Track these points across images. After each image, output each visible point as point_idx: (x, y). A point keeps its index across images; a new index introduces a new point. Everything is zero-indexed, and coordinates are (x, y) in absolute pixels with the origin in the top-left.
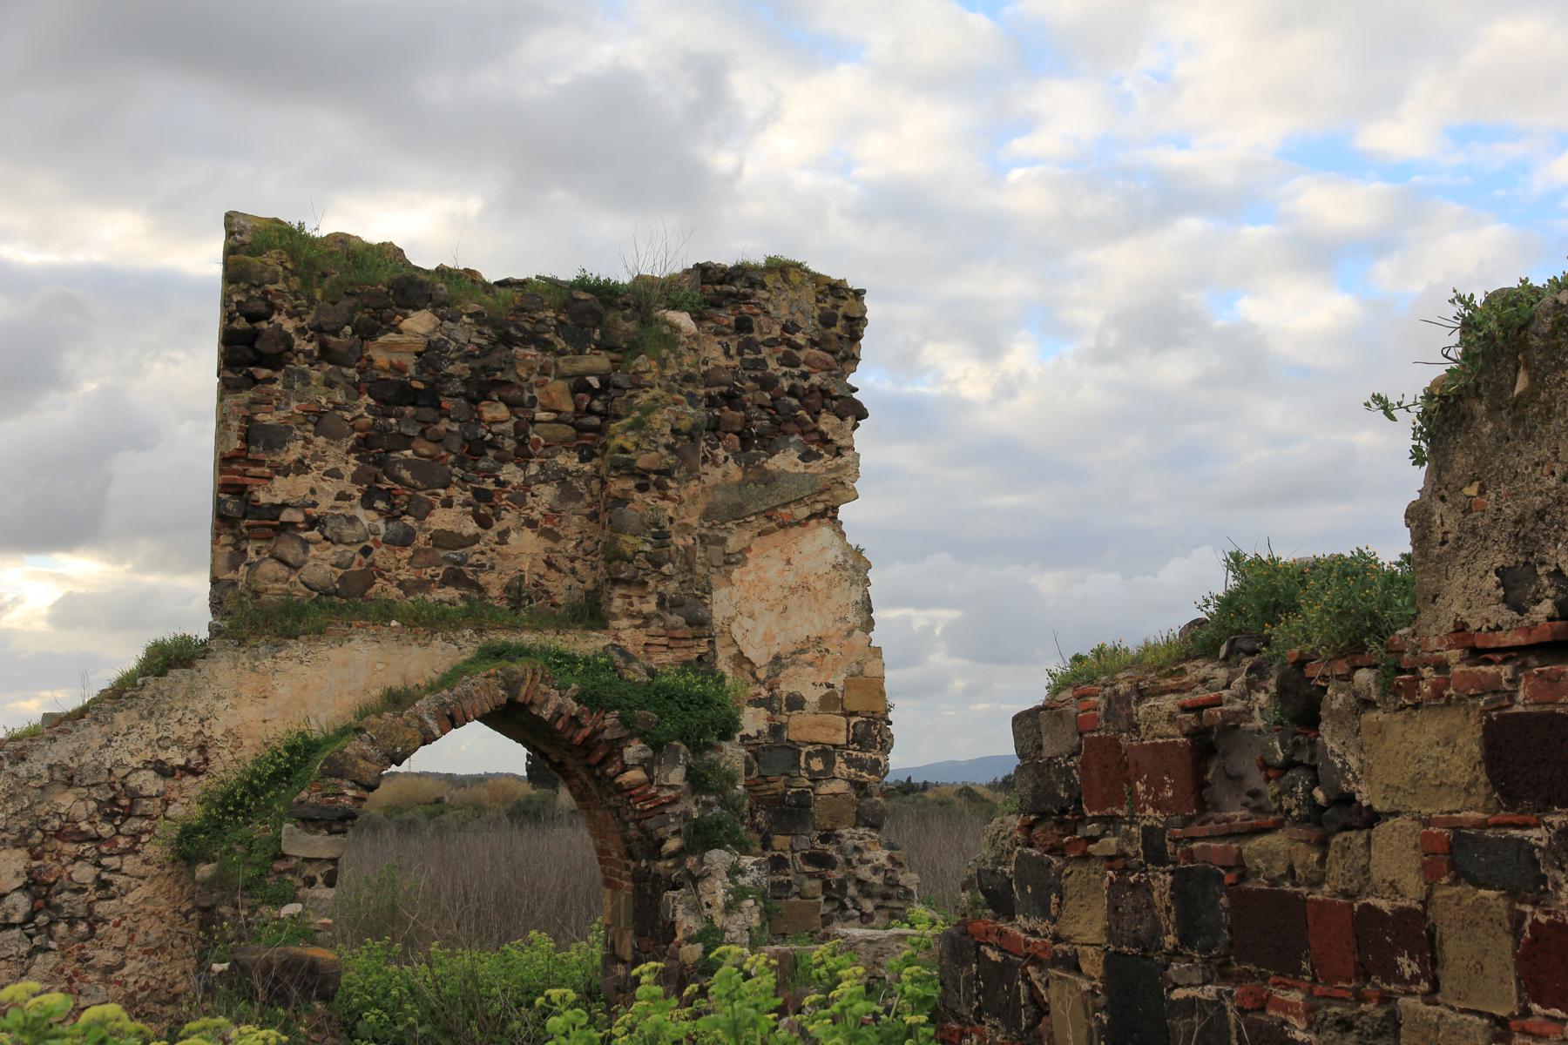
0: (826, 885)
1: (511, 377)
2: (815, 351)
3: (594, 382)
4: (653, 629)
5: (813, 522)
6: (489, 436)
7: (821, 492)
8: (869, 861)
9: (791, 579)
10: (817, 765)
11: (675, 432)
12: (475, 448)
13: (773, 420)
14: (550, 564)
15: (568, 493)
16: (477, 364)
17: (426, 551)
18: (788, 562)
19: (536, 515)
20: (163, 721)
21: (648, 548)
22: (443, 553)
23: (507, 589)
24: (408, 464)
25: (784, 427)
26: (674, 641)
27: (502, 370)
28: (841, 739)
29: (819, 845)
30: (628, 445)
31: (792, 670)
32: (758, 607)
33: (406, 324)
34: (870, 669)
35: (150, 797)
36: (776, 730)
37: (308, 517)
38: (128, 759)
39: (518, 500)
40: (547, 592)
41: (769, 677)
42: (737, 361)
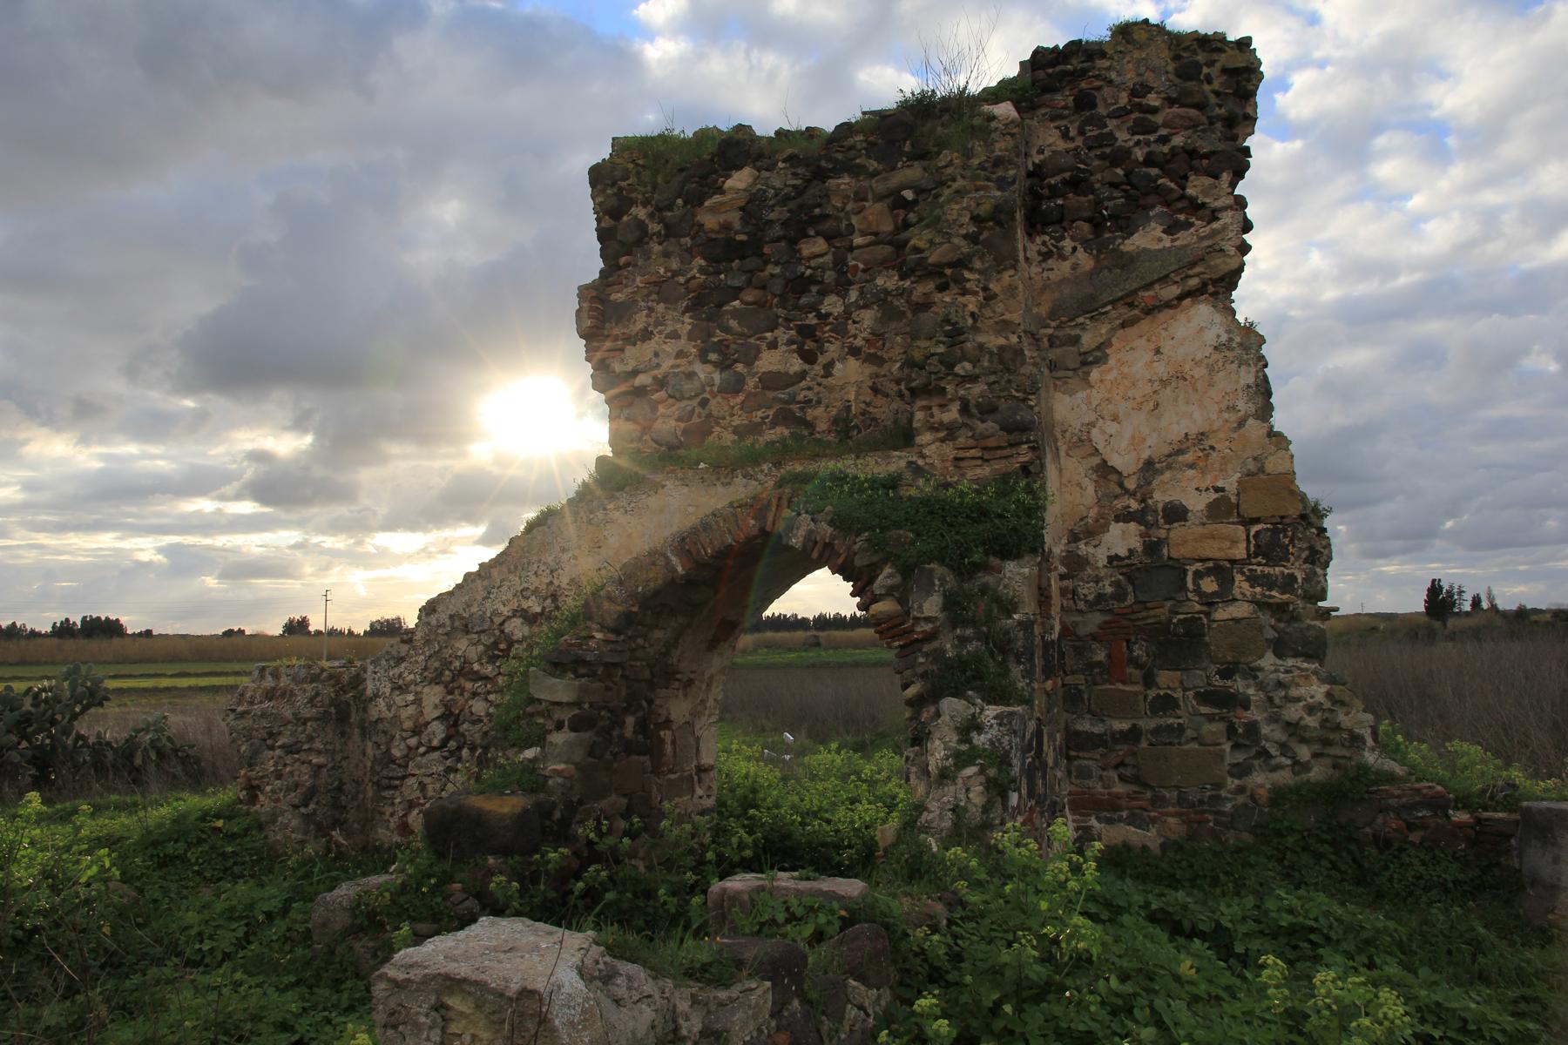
0: (1231, 731)
1: (829, 211)
2: (1176, 110)
3: (908, 194)
4: (961, 441)
5: (1187, 302)
6: (809, 272)
7: (1193, 265)
8: (1298, 700)
9: (1161, 370)
10: (1209, 585)
11: (975, 219)
12: (798, 285)
13: (1128, 196)
14: (875, 390)
15: (889, 313)
16: (792, 205)
17: (755, 395)
18: (1158, 351)
19: (859, 342)
20: (524, 574)
21: (941, 349)
22: (771, 394)
23: (835, 421)
24: (735, 314)
25: (1142, 202)
26: (988, 452)
27: (819, 205)
28: (1240, 552)
29: (1218, 682)
30: (921, 244)
31: (1167, 475)
32: (1122, 407)
33: (729, 183)
34: (1273, 465)
35: (518, 642)
36: (1152, 548)
37: (655, 378)
38: (502, 608)
39: (840, 331)
40: (874, 419)
41: (1139, 486)
42: (1079, 141)
